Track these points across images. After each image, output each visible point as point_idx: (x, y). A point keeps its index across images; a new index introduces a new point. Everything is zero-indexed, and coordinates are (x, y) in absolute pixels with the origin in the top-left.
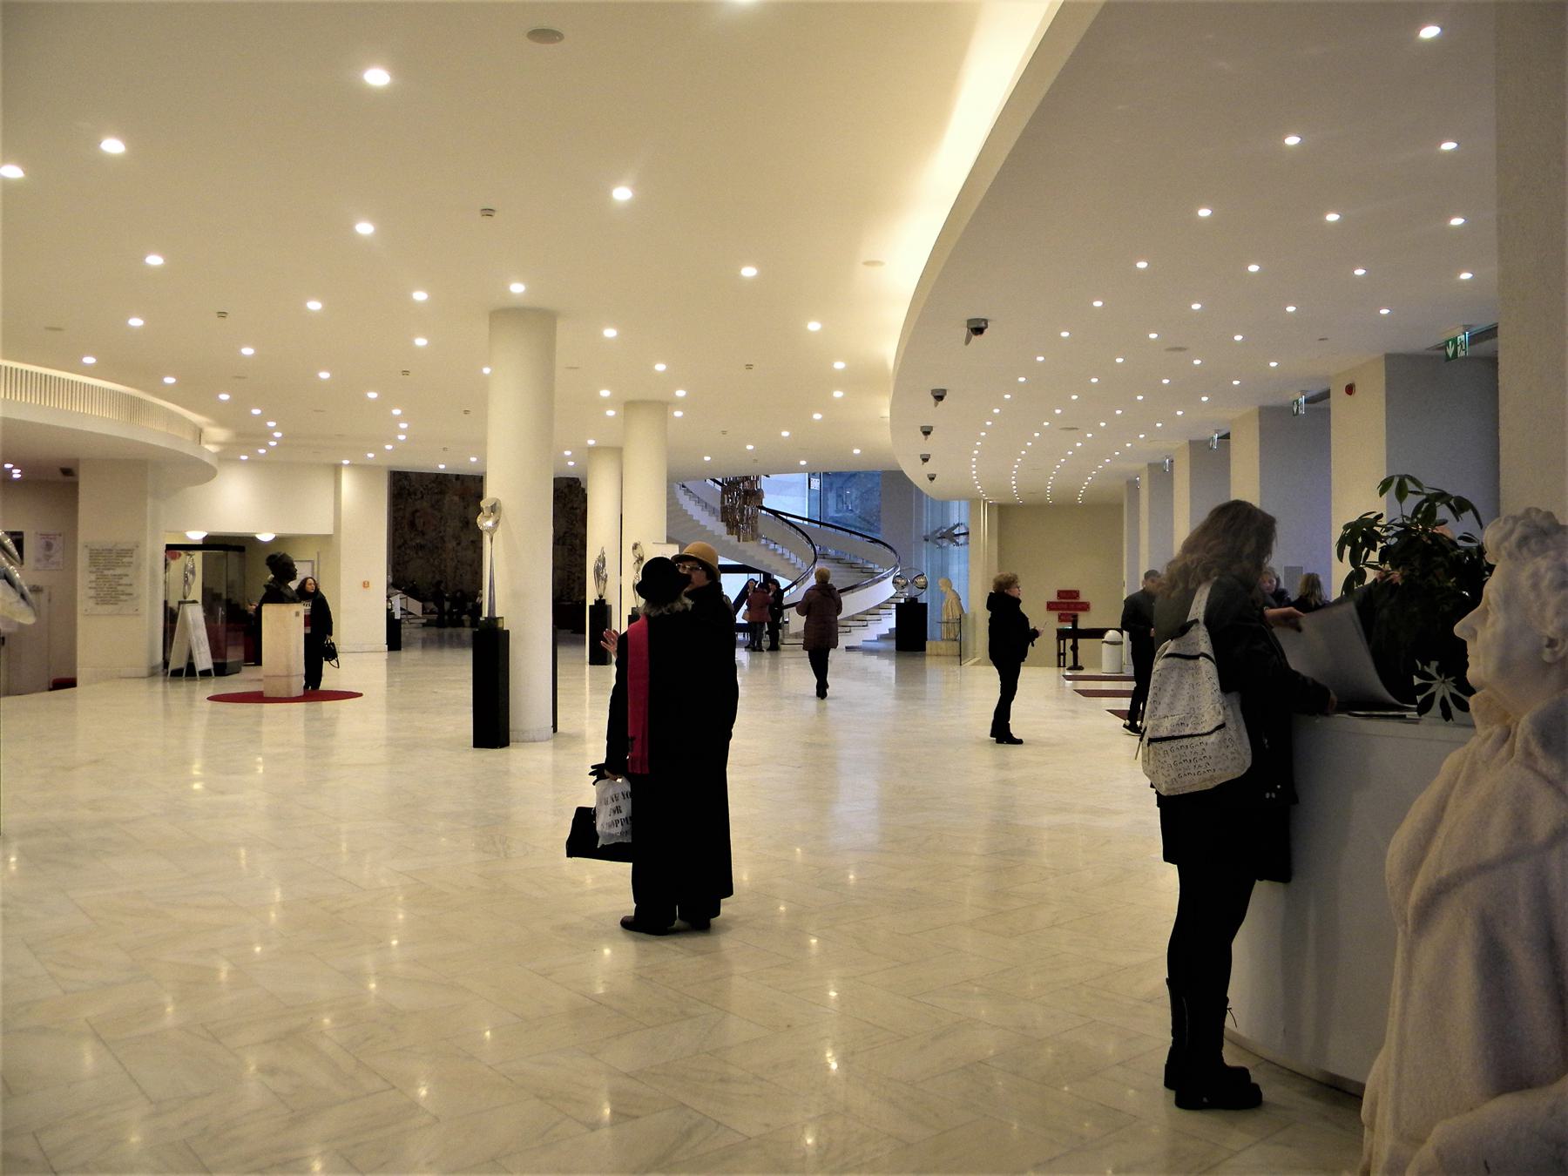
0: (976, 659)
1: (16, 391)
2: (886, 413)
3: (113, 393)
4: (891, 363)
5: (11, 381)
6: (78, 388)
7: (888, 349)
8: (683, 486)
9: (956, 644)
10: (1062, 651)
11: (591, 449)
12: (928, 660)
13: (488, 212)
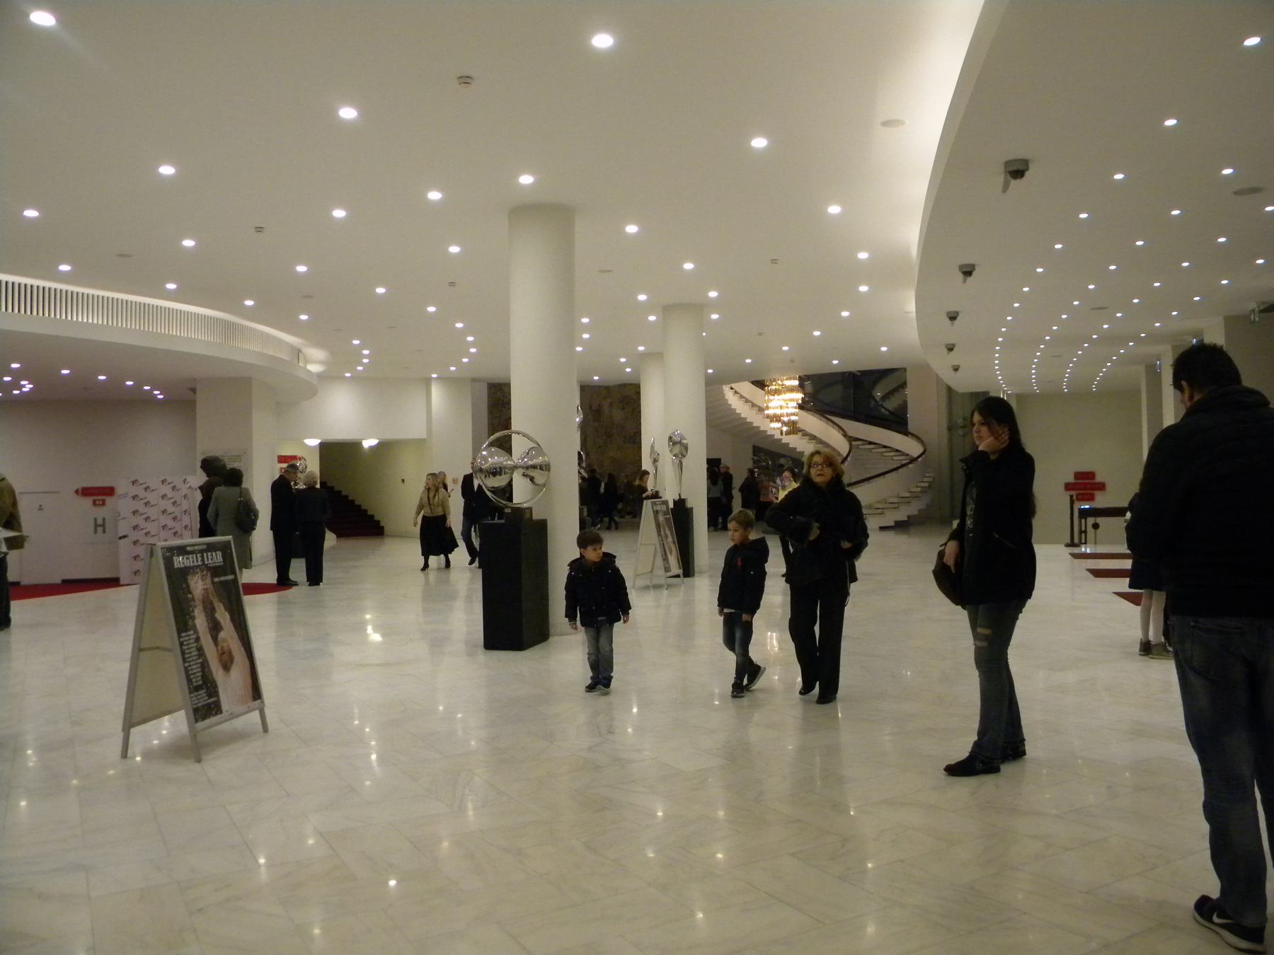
2: (911, 307)
3: (210, 318)
4: (914, 251)
5: (173, 322)
6: (175, 314)
8: (732, 389)
11: (643, 355)
13: (465, 80)
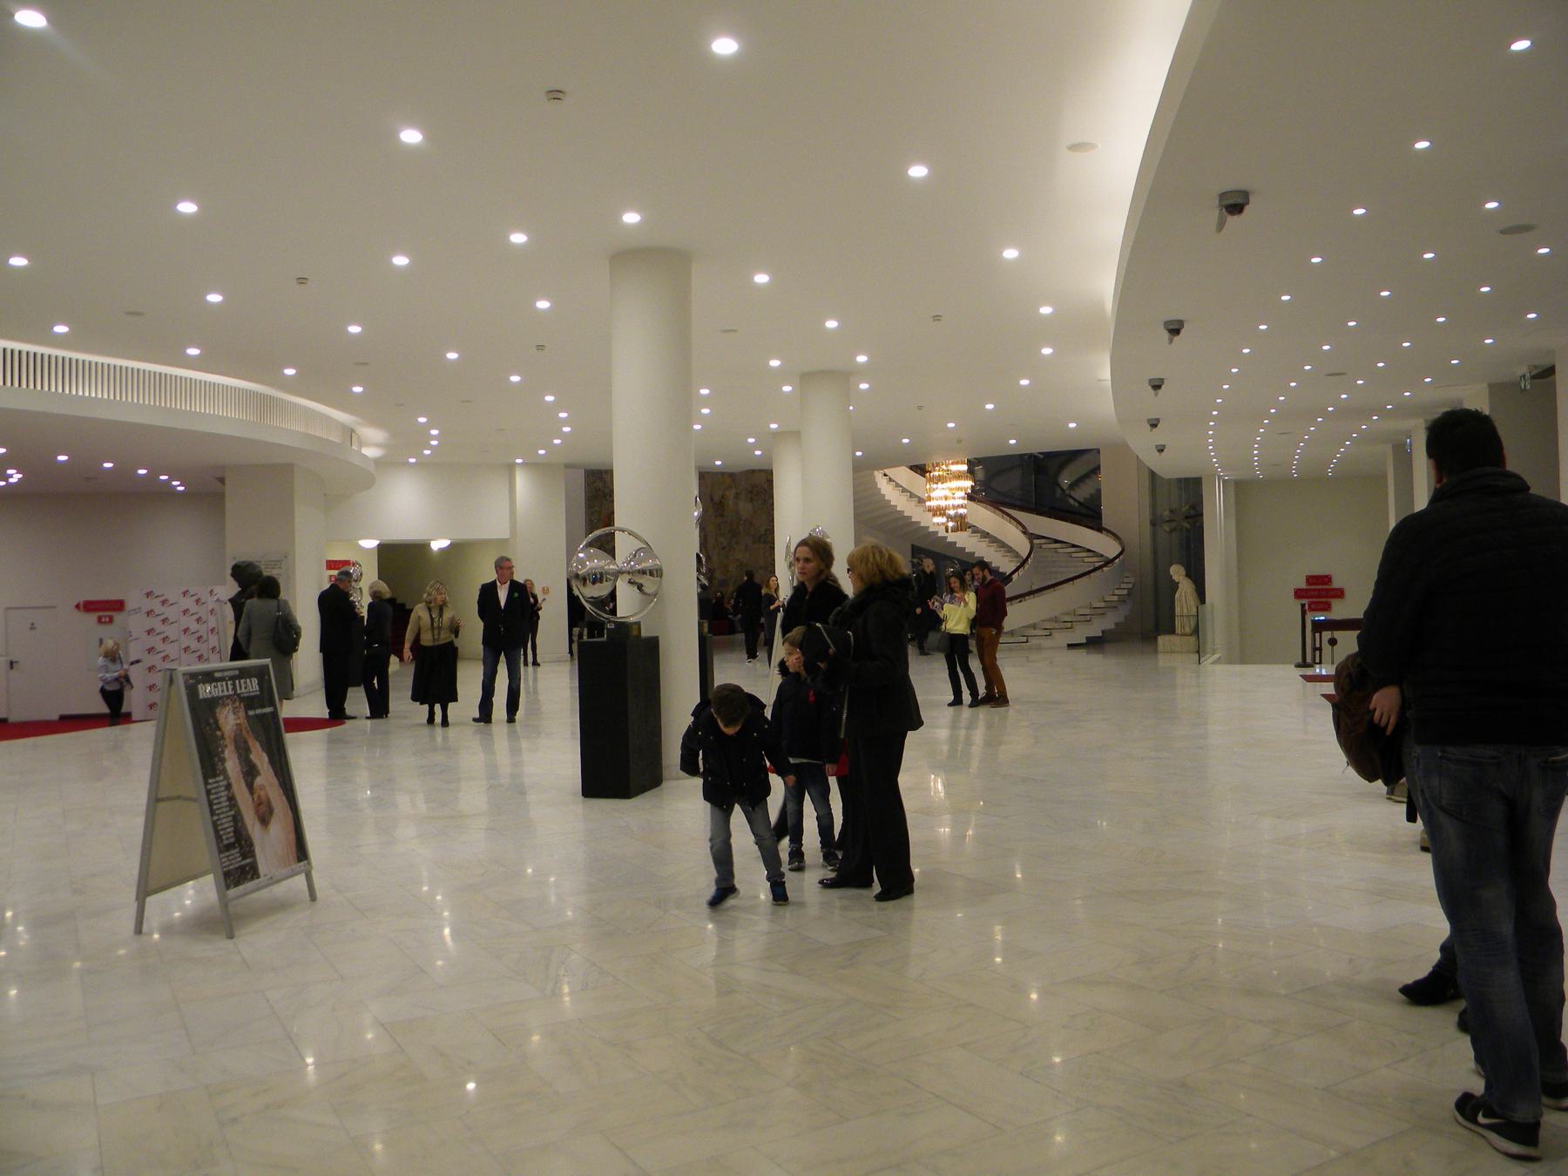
0: (1216, 656)
1: (195, 403)
2: (1105, 373)
7: (1104, 284)
8: (885, 475)
9: (1192, 639)
10: (1318, 646)
11: (776, 434)
12: (1161, 657)
13: (556, 95)
